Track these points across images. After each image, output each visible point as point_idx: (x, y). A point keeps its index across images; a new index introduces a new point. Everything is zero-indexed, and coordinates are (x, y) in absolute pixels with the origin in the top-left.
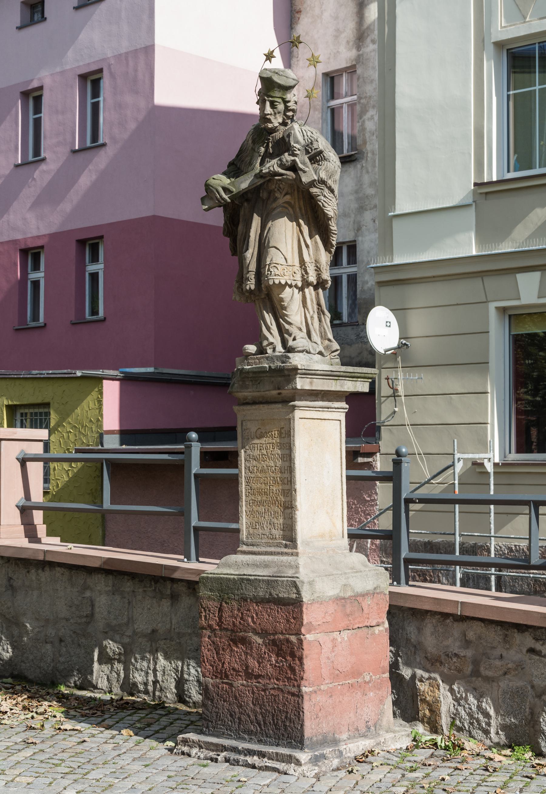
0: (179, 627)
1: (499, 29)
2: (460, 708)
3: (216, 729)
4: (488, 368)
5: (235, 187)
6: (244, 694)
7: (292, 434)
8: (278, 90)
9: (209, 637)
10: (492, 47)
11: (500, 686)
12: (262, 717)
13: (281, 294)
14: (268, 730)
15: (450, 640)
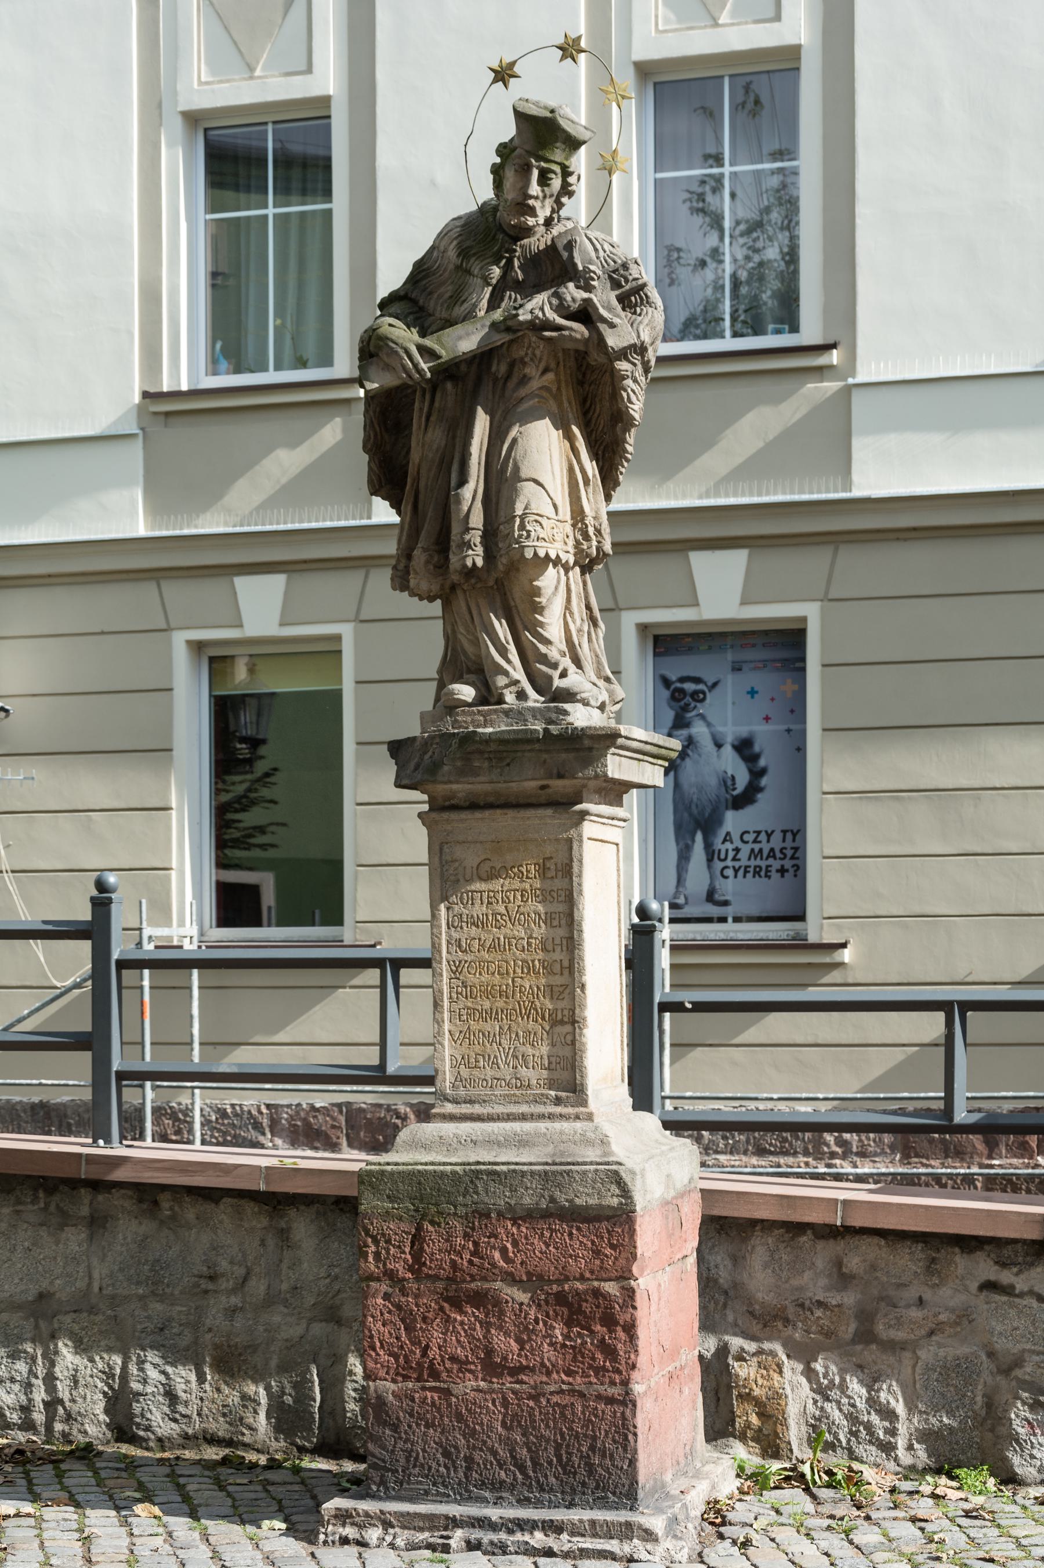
0: (113, 1285)
1: (196, 86)
2: (828, 1406)
3: (405, 1486)
4: (171, 758)
5: (444, 347)
6: (480, 1407)
7: (575, 869)
8: (563, 146)
9: (387, 1297)
10: (178, 123)
11: (918, 1358)
12: (529, 1450)
13: (536, 579)
14: (546, 1477)
15: (807, 1275)
